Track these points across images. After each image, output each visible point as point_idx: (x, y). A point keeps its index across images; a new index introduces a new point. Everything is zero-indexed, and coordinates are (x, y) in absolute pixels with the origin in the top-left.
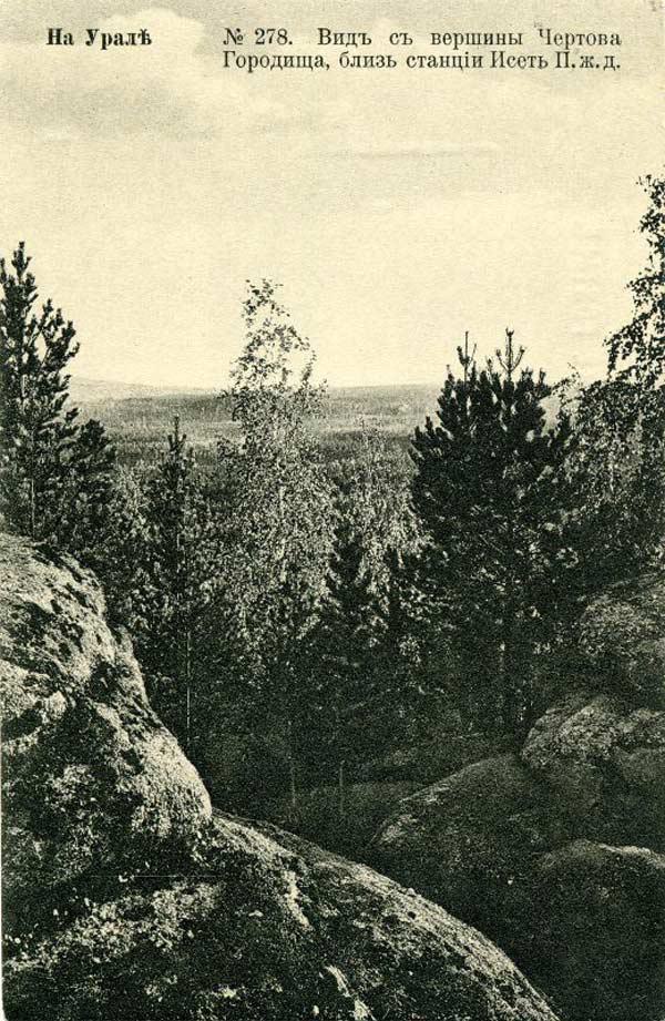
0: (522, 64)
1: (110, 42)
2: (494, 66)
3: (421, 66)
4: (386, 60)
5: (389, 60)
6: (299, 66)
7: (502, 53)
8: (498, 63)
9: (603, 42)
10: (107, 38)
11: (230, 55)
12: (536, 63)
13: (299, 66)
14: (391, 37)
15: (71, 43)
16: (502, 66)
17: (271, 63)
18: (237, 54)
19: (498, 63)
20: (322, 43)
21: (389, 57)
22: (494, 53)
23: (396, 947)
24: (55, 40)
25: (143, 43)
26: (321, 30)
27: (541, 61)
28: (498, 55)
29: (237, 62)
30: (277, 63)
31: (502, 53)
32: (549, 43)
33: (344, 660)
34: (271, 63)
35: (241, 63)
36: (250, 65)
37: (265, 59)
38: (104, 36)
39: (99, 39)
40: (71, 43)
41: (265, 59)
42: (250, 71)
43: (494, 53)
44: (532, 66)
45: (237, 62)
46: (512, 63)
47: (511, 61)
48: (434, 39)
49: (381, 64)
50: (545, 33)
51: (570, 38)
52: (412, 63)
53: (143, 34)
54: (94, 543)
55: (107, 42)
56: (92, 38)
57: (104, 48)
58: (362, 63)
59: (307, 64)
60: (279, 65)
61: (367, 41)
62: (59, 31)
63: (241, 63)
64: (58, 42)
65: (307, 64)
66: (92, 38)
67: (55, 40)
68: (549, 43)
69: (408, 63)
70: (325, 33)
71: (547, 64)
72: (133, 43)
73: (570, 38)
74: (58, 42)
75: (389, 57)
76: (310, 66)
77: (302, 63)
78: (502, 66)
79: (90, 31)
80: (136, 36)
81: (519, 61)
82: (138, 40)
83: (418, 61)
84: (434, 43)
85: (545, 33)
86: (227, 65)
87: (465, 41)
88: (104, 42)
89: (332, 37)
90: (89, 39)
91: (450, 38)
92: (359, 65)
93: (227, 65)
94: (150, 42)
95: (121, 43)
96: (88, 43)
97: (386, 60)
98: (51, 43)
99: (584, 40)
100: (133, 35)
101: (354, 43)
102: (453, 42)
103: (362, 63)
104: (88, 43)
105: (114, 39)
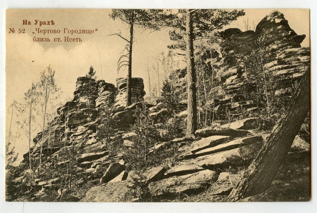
0: (74, 40)
3: (59, 41)
4: (47, 39)
6: (87, 33)
7: (68, 37)
8: (67, 40)
9: (55, 32)
10: (41, 23)
11: (66, 30)
12: (78, 40)
15: (30, 24)
16: (68, 41)
17: (78, 32)
19: (67, 40)
21: (48, 39)
24: (25, 23)
25: (52, 24)
27: (80, 40)
30: (80, 32)
32: (39, 32)
34: (78, 32)
35: (69, 32)
37: (76, 31)
38: (40, 22)
40: (30, 24)
41: (76, 31)
42: (72, 34)
44: (77, 41)
47: (71, 39)
49: (45, 40)
50: (38, 30)
51: (45, 31)
52: (56, 40)
54: (202, 124)
55: (41, 24)
56: (37, 23)
57: (40, 25)
58: (40, 40)
62: (26, 21)
63: (69, 32)
64: (26, 24)
67: (25, 23)
68: (39, 32)
69: (54, 40)
71: (50, 41)
72: (49, 24)
73: (45, 31)
74: (26, 24)
76: (90, 33)
77: (87, 31)
79: (36, 21)
81: (73, 40)
82: (50, 23)
83: (76, 40)
85: (38, 30)
87: (53, 32)
88: (40, 24)
90: (36, 23)
91: (42, 31)
92: (39, 41)
94: (54, 24)
95: (45, 24)
96: (35, 24)
97: (47, 39)
98: (24, 24)
99: (49, 32)
100: (49, 22)
104: (35, 24)
105: (43, 23)
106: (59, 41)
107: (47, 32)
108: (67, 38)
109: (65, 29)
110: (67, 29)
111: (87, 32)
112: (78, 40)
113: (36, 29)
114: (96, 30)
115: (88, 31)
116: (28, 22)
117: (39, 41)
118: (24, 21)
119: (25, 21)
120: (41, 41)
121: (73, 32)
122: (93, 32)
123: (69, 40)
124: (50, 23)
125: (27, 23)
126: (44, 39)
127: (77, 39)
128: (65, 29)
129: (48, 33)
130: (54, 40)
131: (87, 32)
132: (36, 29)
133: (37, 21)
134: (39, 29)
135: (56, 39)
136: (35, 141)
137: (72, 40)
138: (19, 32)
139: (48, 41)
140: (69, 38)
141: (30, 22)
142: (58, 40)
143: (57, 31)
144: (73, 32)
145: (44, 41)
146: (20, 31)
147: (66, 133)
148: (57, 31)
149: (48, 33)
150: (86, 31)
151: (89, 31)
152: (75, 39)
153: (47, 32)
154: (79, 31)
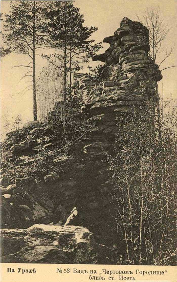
1: (25, 272)
2: (120, 279)
3: (113, 279)
5: (103, 278)
6: (157, 274)
7: (122, 276)
9: (120, 273)
11: (138, 271)
12: (132, 279)
13: (157, 274)
14: (69, 272)
15: (14, 272)
17: (149, 273)
18: (140, 271)
20: (74, 272)
21: (103, 277)
22: (120, 276)
23: (100, 145)
25: (34, 272)
26: (74, 269)
28: (121, 277)
29: (140, 273)
31: (122, 276)
32: (105, 273)
33: (84, 114)
36: (143, 273)
38: (23, 270)
39: (21, 271)
43: (120, 276)
45: (140, 273)
46: (125, 279)
48: (91, 272)
49: (100, 279)
50: (104, 271)
52: (110, 279)
53: (34, 270)
55: (24, 271)
56: (20, 270)
57: (23, 273)
59: (160, 273)
60: (151, 274)
61: (86, 272)
62: (10, 268)
65: (160, 273)
66: (20, 270)
67: (9, 271)
68: (105, 273)
69: (109, 278)
70: (75, 270)
74: (10, 272)
75: (103, 277)
76: (160, 274)
78: (122, 280)
79: (19, 269)
80: (32, 270)
81: (127, 279)
83: (130, 279)
84: (91, 273)
85: (104, 271)
86: (137, 274)
89: (77, 271)
90: (19, 271)
92: (94, 279)
93: (137, 274)
97: (102, 278)
98: (8, 272)
99: (115, 272)
101: (83, 273)
102: (109, 273)
103: (95, 278)
105: (26, 271)
106: (113, 279)
107: (113, 272)
108: (121, 279)
109: (137, 270)
110: (139, 270)
111: (158, 273)
112: (132, 279)
113: (103, 270)
114: (135, 279)
115: (157, 272)
116: (12, 270)
117: (94, 279)
118: (8, 268)
119: (9, 269)
120: (96, 279)
121: (144, 273)
122: (163, 273)
123: (123, 279)
124: (32, 271)
125: (11, 271)
126: (99, 278)
127: (131, 277)
128: (137, 270)
129: (114, 273)
130: (109, 278)
131: (158, 273)
132: (103, 270)
133: (20, 269)
134: (105, 270)
135: (111, 278)
136: (85, 91)
137: (126, 278)
138: (64, 272)
139: (103, 279)
140: (123, 277)
141: (14, 270)
142: (112, 278)
143: (122, 272)
144: (144, 273)
145: (99, 279)
146: (65, 271)
147: (79, 14)
148: (122, 272)
149: (114, 273)
150: (156, 272)
151: (158, 272)
152: (163, 272)
153: (113, 272)
154: (149, 272)
